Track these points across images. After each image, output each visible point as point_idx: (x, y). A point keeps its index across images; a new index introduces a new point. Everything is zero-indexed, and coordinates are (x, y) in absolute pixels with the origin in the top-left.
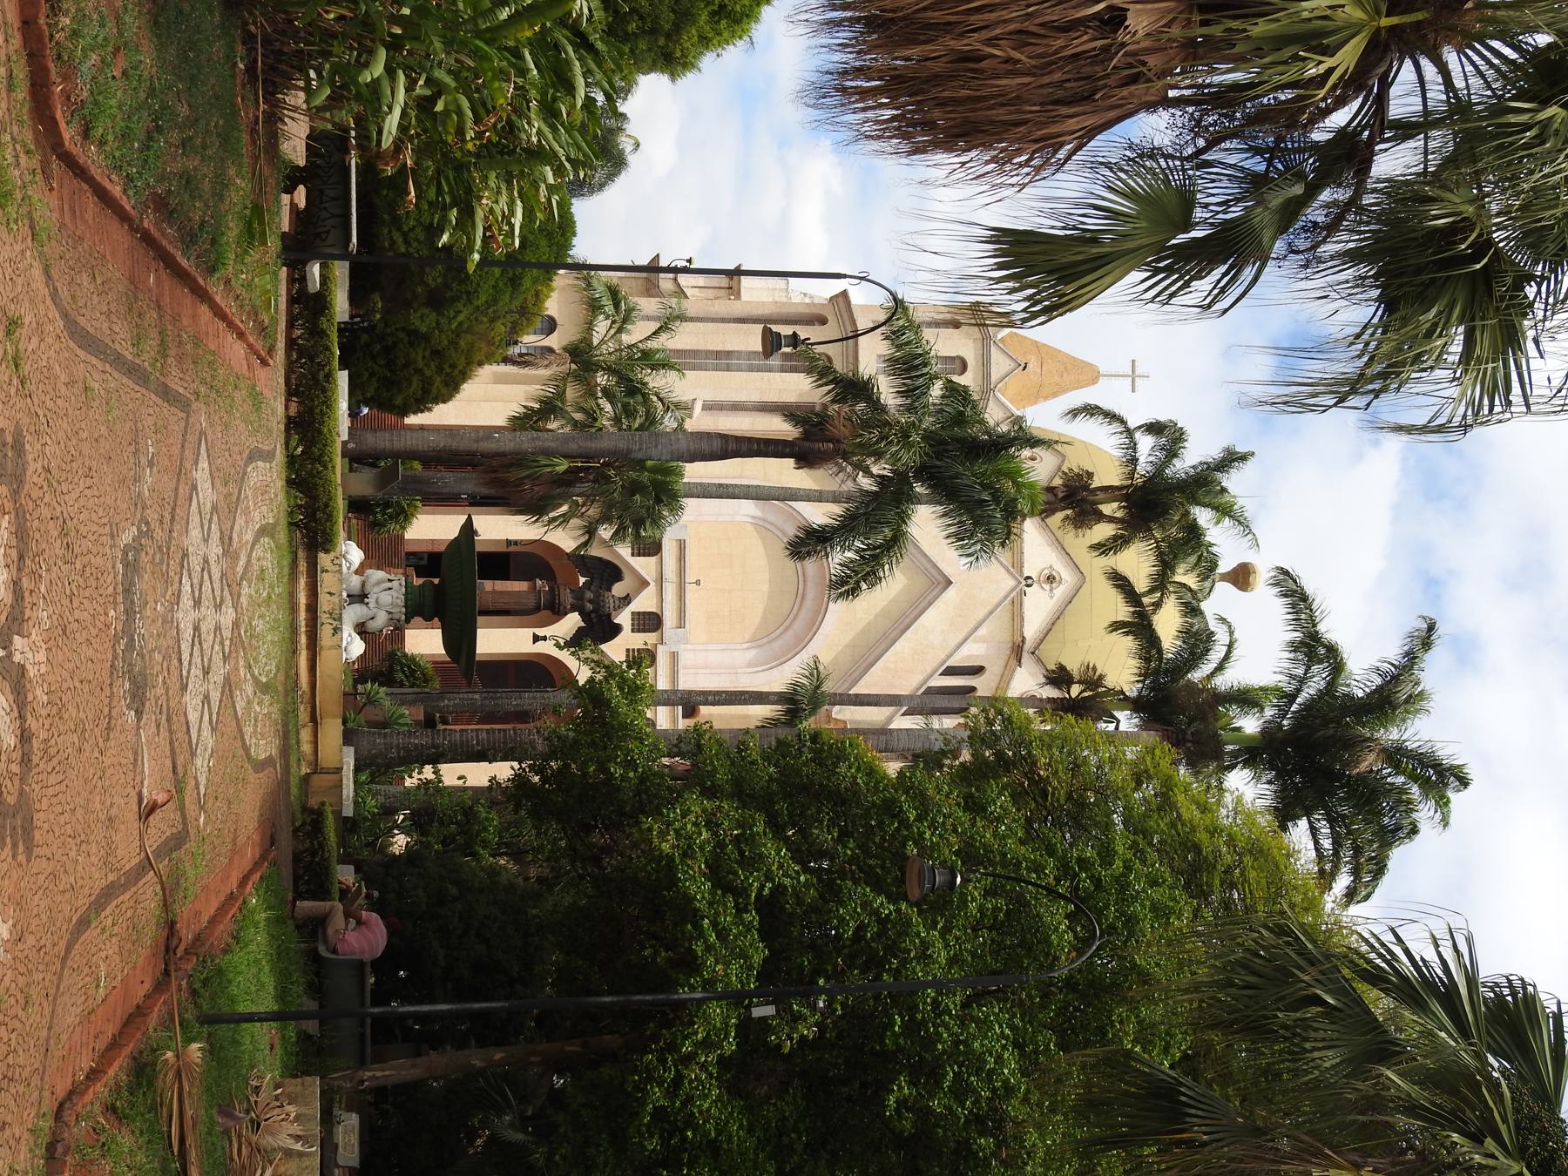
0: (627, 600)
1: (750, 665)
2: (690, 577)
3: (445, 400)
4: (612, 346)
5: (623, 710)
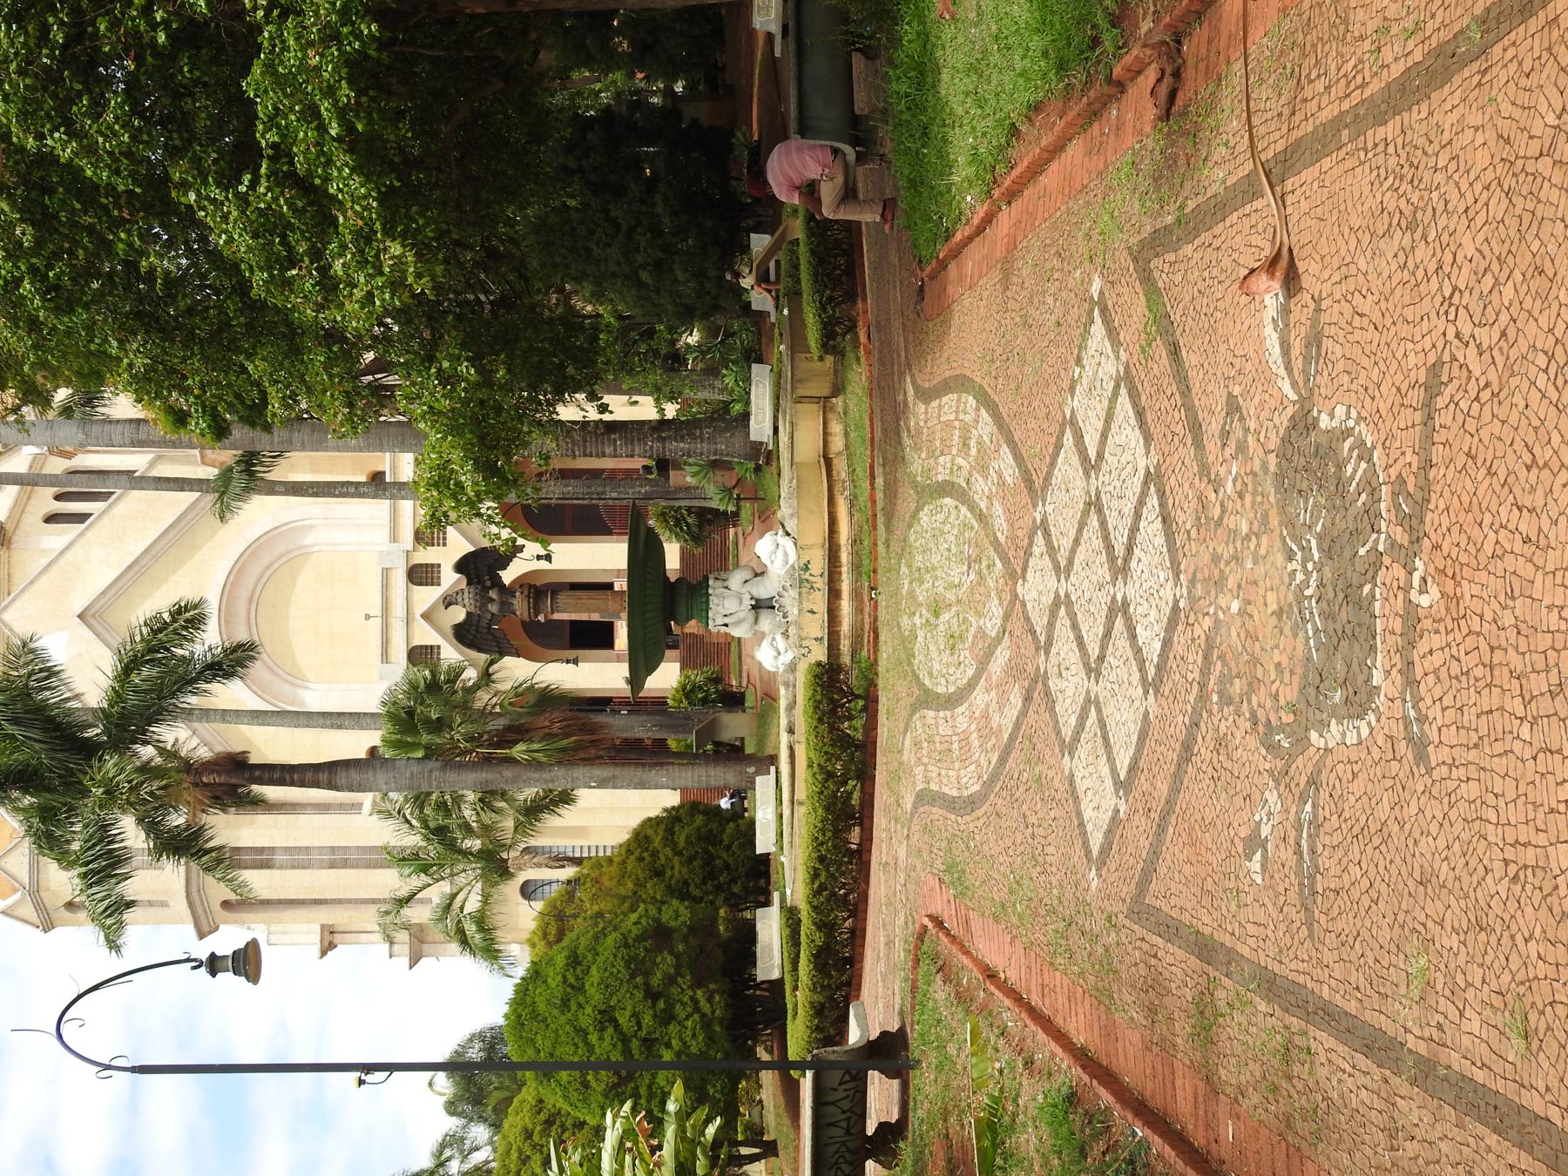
0: (448, 601)
1: (311, 527)
2: (376, 623)
3: (650, 819)
4: (461, 880)
5: (456, 455)
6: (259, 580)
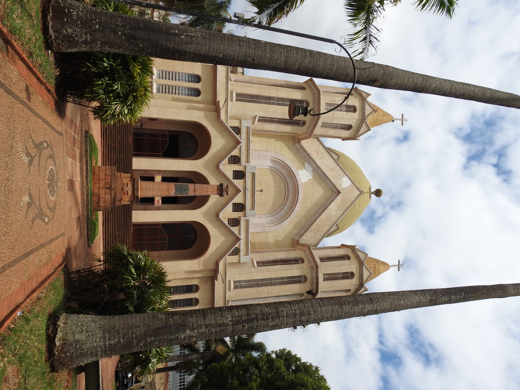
2: (257, 188)
6: (285, 205)
